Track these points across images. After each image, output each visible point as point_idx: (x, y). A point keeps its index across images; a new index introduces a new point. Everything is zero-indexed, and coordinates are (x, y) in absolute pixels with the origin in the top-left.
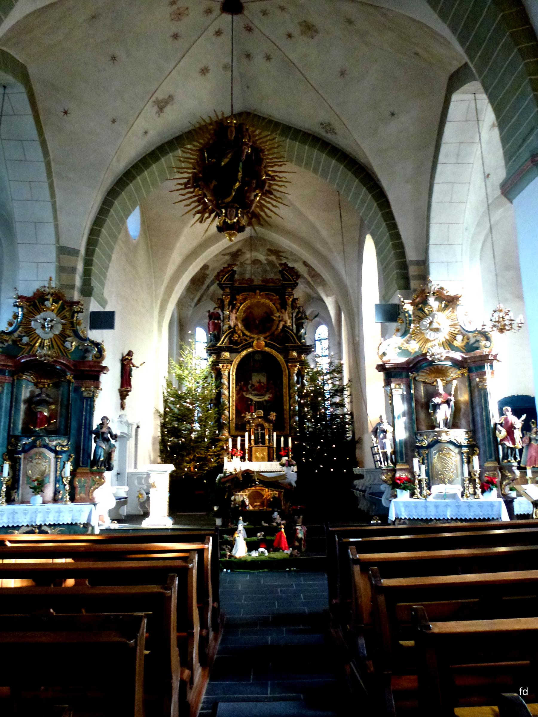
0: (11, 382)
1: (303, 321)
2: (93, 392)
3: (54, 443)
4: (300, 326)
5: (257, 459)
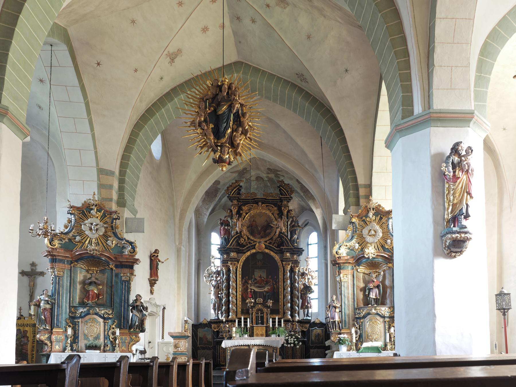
0: (70, 269)
1: (296, 228)
2: (130, 277)
3: (103, 312)
4: (293, 233)
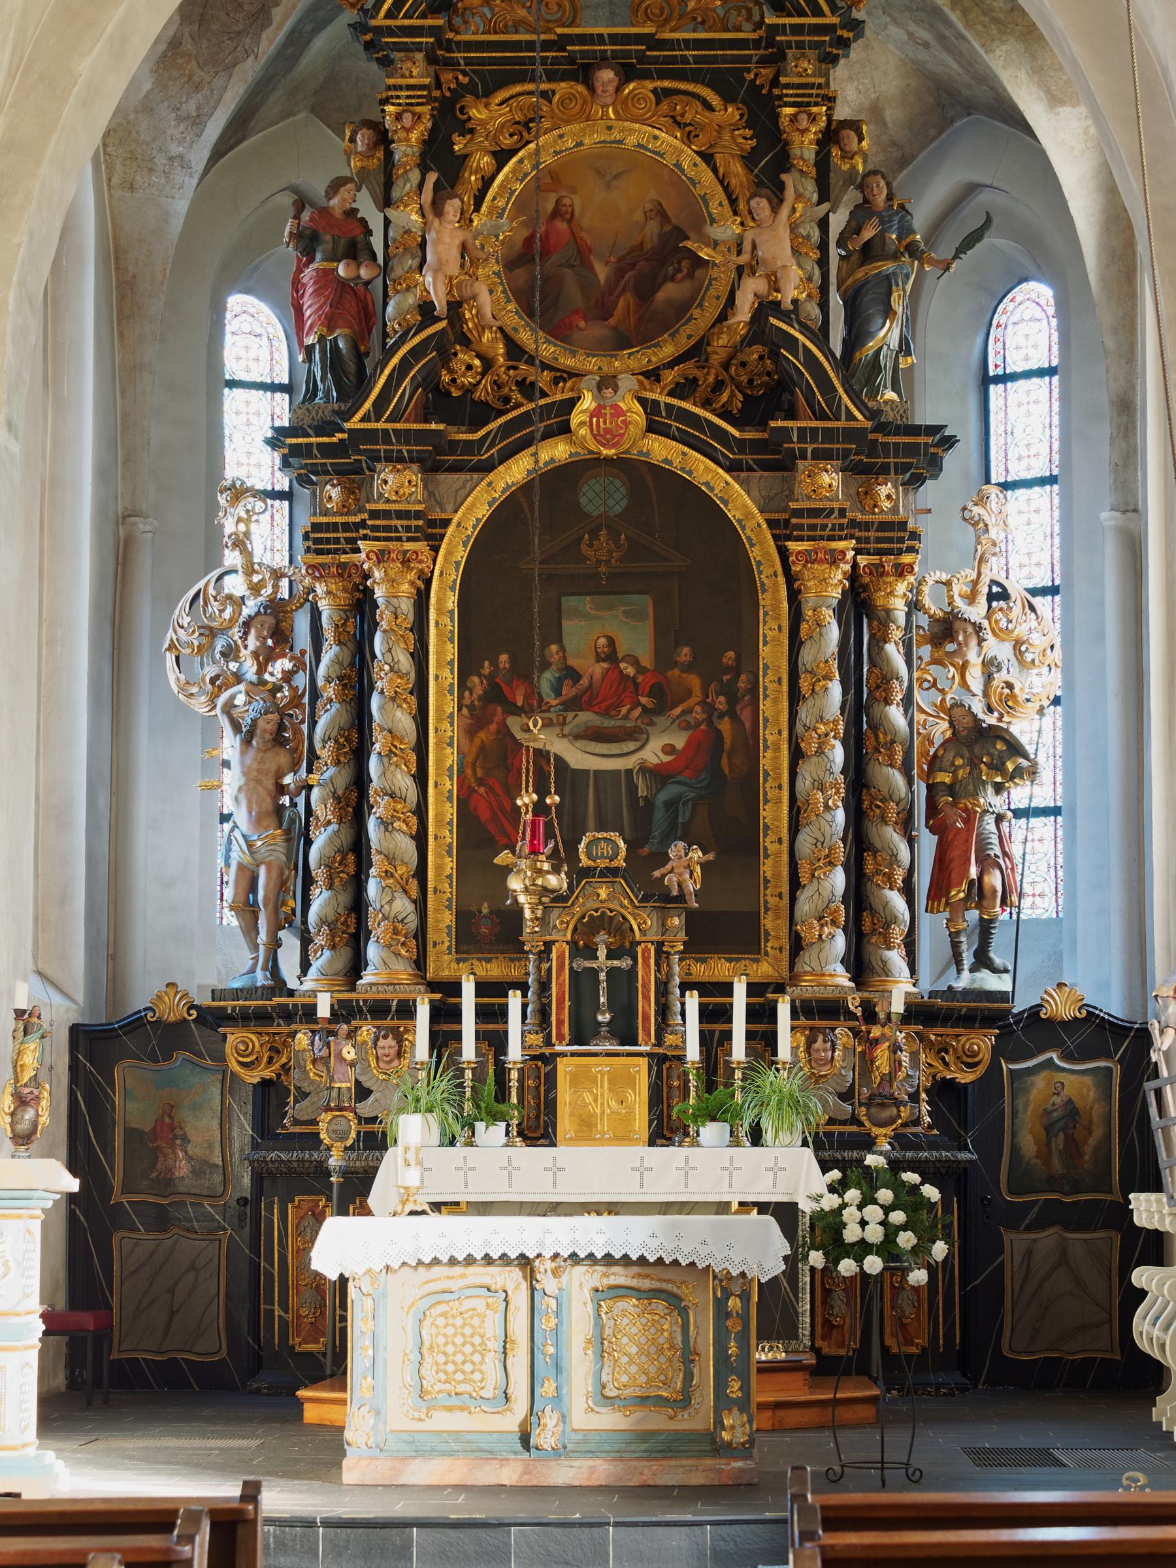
5: (587, 1131)
